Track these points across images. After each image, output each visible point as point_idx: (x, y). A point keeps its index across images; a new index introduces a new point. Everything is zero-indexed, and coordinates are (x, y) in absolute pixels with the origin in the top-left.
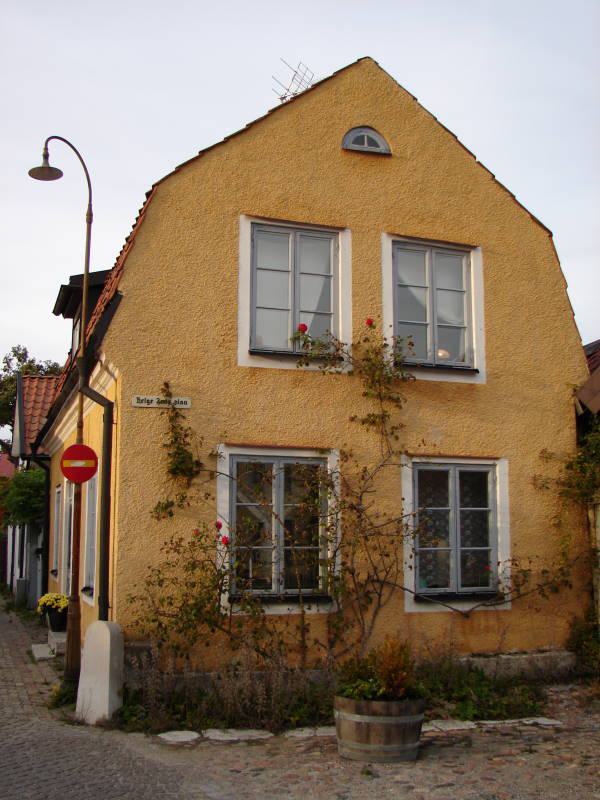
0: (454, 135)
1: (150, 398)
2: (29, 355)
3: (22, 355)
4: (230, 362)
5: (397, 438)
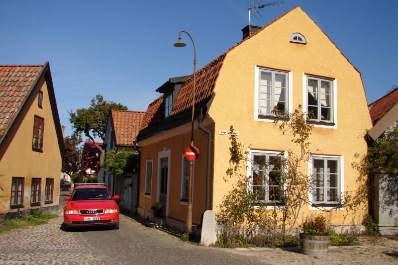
0: (342, 54)
1: (225, 131)
2: (104, 99)
3: (100, 99)
4: (252, 119)
5: (307, 148)
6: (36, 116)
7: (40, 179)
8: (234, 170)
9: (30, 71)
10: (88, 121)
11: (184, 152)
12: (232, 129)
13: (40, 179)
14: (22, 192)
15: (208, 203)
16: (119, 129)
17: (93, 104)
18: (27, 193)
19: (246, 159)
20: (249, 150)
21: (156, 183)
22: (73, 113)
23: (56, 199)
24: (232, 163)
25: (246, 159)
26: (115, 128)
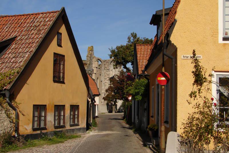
1: (187, 56)
4: (216, 41)
6: (55, 54)
7: (64, 106)
8: (197, 93)
9: (49, 17)
10: (124, 55)
11: (157, 77)
12: (194, 52)
13: (64, 106)
14: (45, 117)
15: (173, 125)
16: (141, 61)
17: (129, 41)
18: (50, 118)
19: (210, 82)
20: (213, 73)
21: (91, 112)
22: (113, 50)
23: (82, 123)
24: (195, 86)
25: (210, 82)
26: (138, 60)
